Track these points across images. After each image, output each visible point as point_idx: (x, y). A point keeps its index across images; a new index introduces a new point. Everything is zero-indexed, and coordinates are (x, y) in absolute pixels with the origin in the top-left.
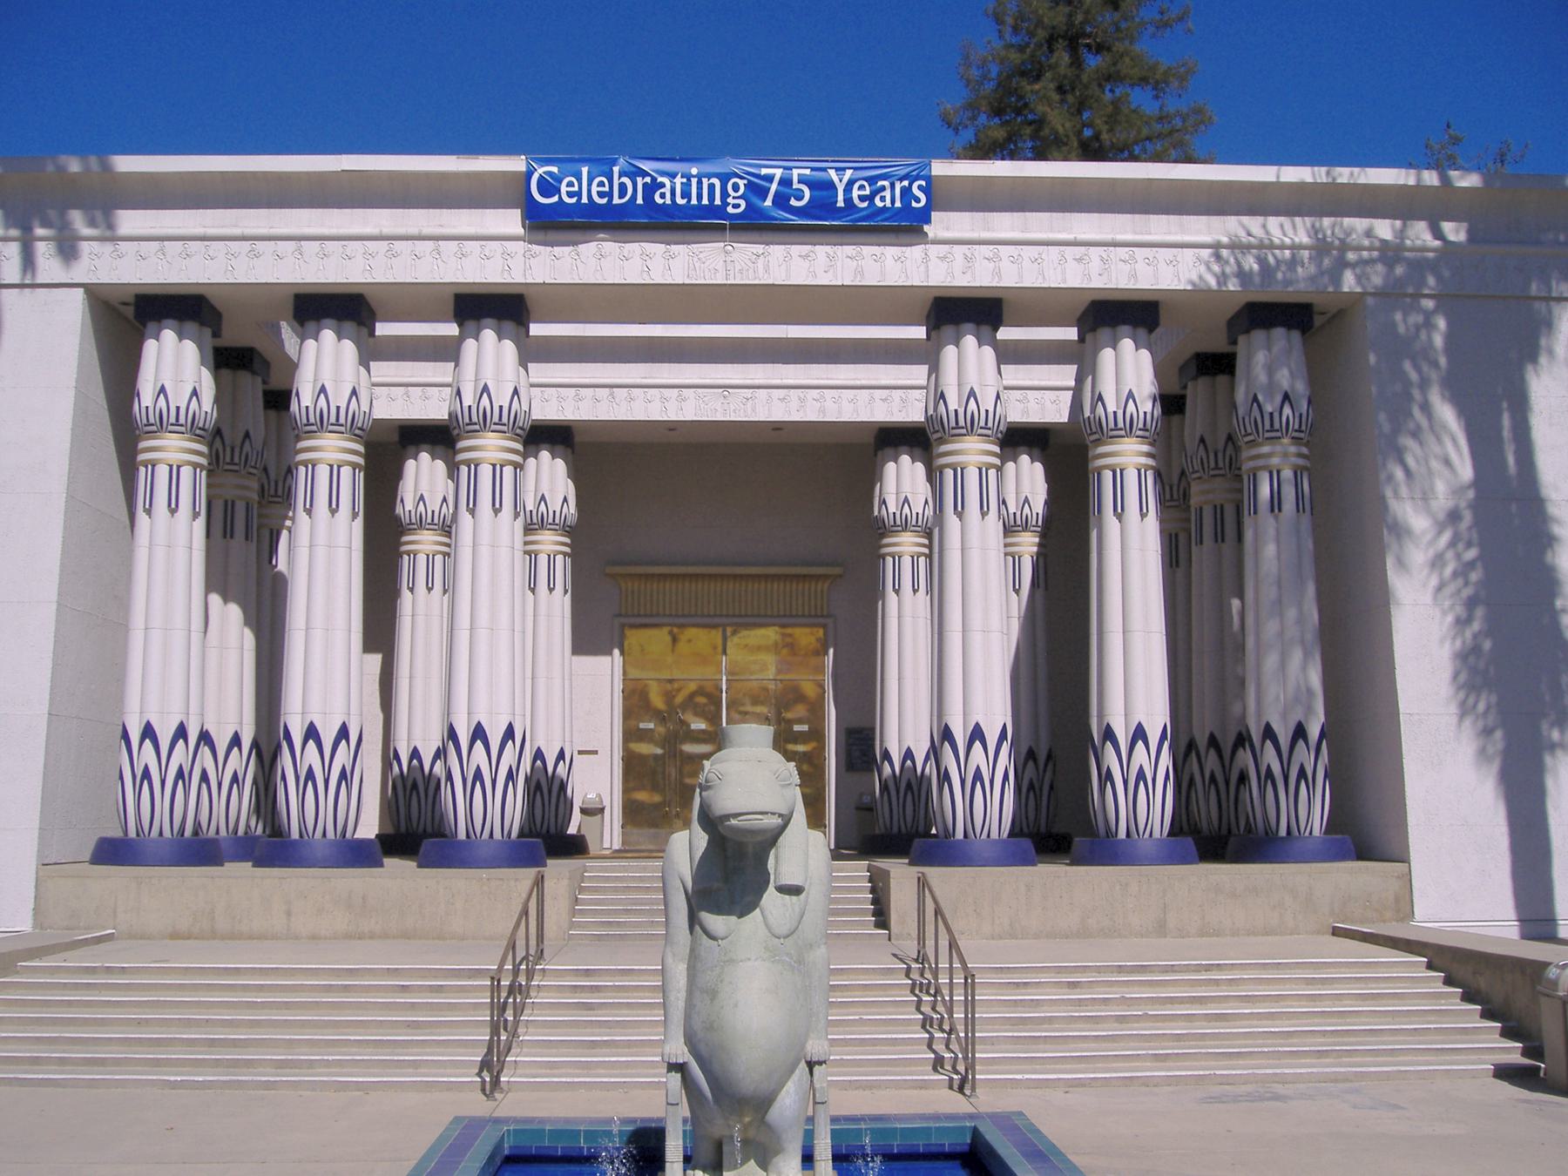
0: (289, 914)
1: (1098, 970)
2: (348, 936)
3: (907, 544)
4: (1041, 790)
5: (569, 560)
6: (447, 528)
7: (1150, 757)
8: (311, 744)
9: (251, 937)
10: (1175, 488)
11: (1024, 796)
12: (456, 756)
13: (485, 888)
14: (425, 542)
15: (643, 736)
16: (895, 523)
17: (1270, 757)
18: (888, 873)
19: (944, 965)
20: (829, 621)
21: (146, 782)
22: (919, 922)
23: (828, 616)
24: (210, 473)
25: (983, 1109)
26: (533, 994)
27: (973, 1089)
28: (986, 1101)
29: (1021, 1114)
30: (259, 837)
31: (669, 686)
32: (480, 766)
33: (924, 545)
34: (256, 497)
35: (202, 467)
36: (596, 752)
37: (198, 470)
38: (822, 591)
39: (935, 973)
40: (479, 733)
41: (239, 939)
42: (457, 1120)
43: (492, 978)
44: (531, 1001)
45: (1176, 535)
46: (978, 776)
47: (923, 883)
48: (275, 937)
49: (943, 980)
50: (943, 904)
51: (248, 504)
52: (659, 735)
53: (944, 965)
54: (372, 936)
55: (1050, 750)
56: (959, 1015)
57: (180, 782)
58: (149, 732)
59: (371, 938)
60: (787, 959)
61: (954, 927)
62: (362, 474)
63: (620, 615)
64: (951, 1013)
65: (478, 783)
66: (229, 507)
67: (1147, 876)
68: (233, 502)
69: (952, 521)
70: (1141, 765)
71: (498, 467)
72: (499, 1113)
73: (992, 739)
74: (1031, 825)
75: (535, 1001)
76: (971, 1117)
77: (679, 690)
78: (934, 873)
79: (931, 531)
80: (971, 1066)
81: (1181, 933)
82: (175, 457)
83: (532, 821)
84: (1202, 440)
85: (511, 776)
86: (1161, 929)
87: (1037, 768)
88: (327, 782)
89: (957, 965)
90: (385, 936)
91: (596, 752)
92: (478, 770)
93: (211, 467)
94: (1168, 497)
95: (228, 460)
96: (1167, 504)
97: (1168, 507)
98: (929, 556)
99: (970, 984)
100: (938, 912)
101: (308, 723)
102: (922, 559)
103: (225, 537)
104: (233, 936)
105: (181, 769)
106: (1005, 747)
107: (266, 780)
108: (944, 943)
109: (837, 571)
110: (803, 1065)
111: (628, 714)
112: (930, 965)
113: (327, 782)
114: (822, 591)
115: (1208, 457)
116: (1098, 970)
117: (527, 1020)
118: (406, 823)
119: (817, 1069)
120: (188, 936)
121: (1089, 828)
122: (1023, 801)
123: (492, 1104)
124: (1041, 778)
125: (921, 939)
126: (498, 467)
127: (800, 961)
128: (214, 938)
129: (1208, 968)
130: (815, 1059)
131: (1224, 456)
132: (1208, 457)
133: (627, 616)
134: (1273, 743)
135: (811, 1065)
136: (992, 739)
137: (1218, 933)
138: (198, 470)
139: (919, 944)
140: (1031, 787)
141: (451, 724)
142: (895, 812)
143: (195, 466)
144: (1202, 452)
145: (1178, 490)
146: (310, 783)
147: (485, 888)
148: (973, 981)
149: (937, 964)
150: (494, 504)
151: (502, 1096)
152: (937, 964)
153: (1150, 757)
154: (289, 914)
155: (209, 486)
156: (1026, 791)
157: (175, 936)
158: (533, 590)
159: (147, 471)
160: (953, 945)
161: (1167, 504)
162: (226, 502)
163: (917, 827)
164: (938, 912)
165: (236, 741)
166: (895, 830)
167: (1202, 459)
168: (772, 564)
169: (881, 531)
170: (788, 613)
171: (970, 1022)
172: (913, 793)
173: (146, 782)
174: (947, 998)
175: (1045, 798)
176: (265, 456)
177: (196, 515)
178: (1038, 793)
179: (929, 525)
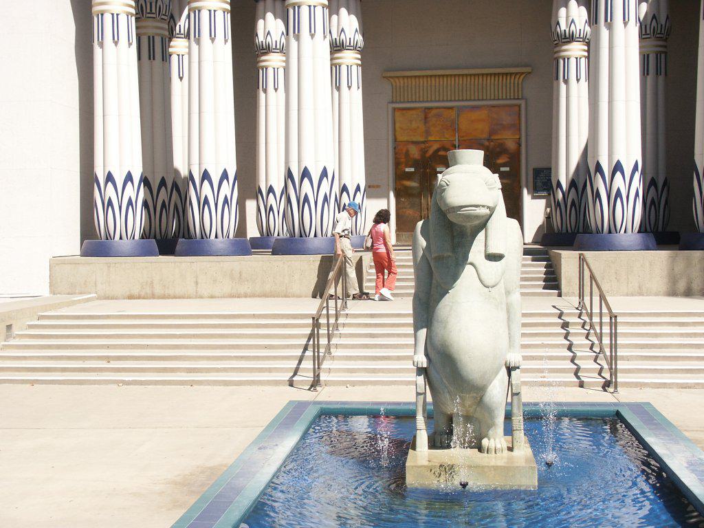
0: (197, 283)
2: (232, 296)
3: (575, 50)
4: (659, 204)
5: (360, 68)
6: (284, 50)
7: (276, 199)
8: (206, 182)
9: (175, 297)
10: (648, 27)
11: (647, 209)
13: (312, 266)
14: (273, 61)
15: (409, 176)
16: (180, 32)
18: (561, 254)
19: (596, 310)
20: (523, 103)
22: (580, 285)
23: (522, 99)
24: (137, 20)
25: (623, 400)
27: (616, 387)
28: (624, 396)
29: (649, 404)
31: (423, 146)
33: (585, 51)
34: (167, 33)
35: (132, 15)
36: (378, 186)
37: (130, 16)
38: (518, 83)
39: (591, 316)
40: (305, 174)
41: (169, 298)
42: (291, 402)
43: (313, 318)
45: (648, 55)
46: (619, 194)
47: (582, 260)
48: (189, 297)
49: (596, 319)
50: (594, 271)
51: (162, 38)
53: (596, 310)
54: (246, 296)
55: (666, 178)
56: (606, 341)
57: (130, 207)
58: (110, 178)
59: (246, 297)
61: (603, 288)
62: (229, 14)
63: (392, 102)
64: (600, 340)
66: (151, 40)
68: (153, 37)
69: (604, 33)
70: (226, 195)
71: (312, 8)
72: (319, 399)
73: (628, 171)
74: (652, 226)
76: (615, 404)
77: (430, 147)
78: (589, 255)
79: (591, 45)
80: (614, 372)
85: (326, 199)
87: (657, 191)
88: (216, 205)
89: (605, 310)
90: (253, 296)
91: (378, 186)
93: (138, 16)
94: (644, 33)
95: (148, 11)
96: (643, 37)
97: (644, 38)
98: (588, 57)
99: (614, 323)
100: (592, 277)
102: (583, 59)
103: (150, 59)
104: (164, 297)
105: (130, 200)
106: (637, 176)
108: (596, 299)
109: (528, 69)
110: (504, 370)
111: (397, 164)
112: (586, 309)
113: (216, 205)
114: (518, 83)
119: (513, 373)
120: (139, 297)
121: (587, 229)
123: (315, 393)
125: (581, 295)
126: (312, 8)
128: (154, 298)
130: (512, 365)
131: (650, 27)
133: (396, 102)
135: (510, 370)
136: (628, 171)
138: (130, 16)
139: (580, 298)
140: (653, 202)
141: (289, 169)
142: (564, 221)
145: (650, 27)
146: (306, 204)
147: (312, 266)
148: (616, 320)
149: (591, 309)
150: (310, 31)
151: (321, 388)
152: (591, 309)
153: (276, 199)
154: (197, 283)
155: (137, 28)
156: (650, 205)
157: (131, 297)
158: (338, 89)
160: (602, 297)
161: (643, 37)
162: (149, 37)
163: (578, 229)
164: (592, 277)
165: (225, 176)
166: (564, 231)
168: (457, 68)
169: (556, 42)
170: (453, 99)
171: (614, 346)
172: (273, 213)
174: (598, 331)
175: (662, 210)
176: (171, 7)
178: (577, 207)
179: (588, 37)
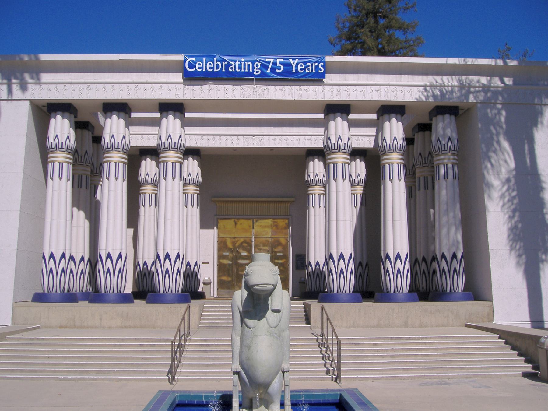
0: (101, 319)
1: (384, 339)
2: (122, 327)
3: (317, 190)
4: (364, 276)
5: (199, 196)
6: (156, 185)
7: (402, 265)
8: (109, 260)
9: (88, 328)
10: (411, 171)
11: (358, 278)
12: (159, 264)
13: (170, 310)
14: (148, 189)
15: (225, 257)
17: (444, 264)
18: (310, 305)
19: (330, 337)
20: (290, 217)
21: (51, 273)
22: (321, 322)
23: (290, 215)
24: (73, 165)
25: (343, 388)
26: (186, 347)
27: (340, 381)
28: (345, 385)
29: (357, 389)
30: (90, 292)
31: (234, 240)
32: (168, 268)
33: (323, 191)
34: (89, 174)
35: (70, 163)
36: (208, 263)
37: (69, 164)
38: (287, 207)
39: (327, 340)
40: (167, 256)
41: (84, 328)
42: (160, 391)
43: (172, 342)
44: (186, 350)
45: (411, 187)
46: (342, 271)
47: (322, 309)
48: (96, 328)
49: (330, 343)
50: (329, 316)
51: (87, 176)
52: (230, 257)
53: (330, 337)
54: (130, 327)
55: (367, 262)
56: (335, 355)
57: (63, 273)
58: (52, 256)
59: (130, 328)
60: (275, 335)
61: (333, 324)
62: (126, 166)
63: (217, 215)
64: (332, 354)
65: (167, 274)
66: (80, 177)
67: (401, 306)
68: (81, 175)
69: (333, 182)
70: (399, 267)
71: (174, 163)
72: (174, 389)
73: (347, 258)
74: (360, 288)
75: (187, 350)
76: (339, 390)
77: (237, 241)
78: (326, 305)
79: (325, 186)
80: (339, 373)
81: (413, 326)
82: (61, 160)
83: (186, 287)
84: (420, 154)
85: (178, 271)
86: (406, 325)
87: (362, 269)
88: (114, 273)
89: (334, 337)
90: (135, 327)
91: (208, 263)
92: (167, 269)
93: (74, 163)
94: (408, 174)
95: (80, 161)
96: (408, 176)
97: (408, 177)
98: (325, 194)
99: (339, 344)
100: (328, 319)
101: (108, 253)
102: (322, 195)
103: (79, 188)
104: (81, 327)
105: (63, 269)
106: (351, 261)
107: (93, 273)
108: (330, 329)
109: (292, 199)
110: (281, 372)
111: (219, 250)
112: (325, 337)
113: (114, 273)
114: (287, 207)
115: (422, 160)
116: (384, 339)
117: (184, 357)
118: (142, 288)
119: (285, 373)
120: (66, 327)
121: (380, 290)
122: (358, 280)
123: (172, 386)
124: (364, 272)
125: (322, 328)
126: (174, 163)
127: (280, 336)
128: (75, 328)
129: (422, 338)
130: (285, 370)
131: (428, 159)
132: (422, 160)
133: (219, 215)
134: (445, 260)
135: (283, 372)
136: (347, 258)
137: (426, 326)
138: (69, 164)
139: (321, 330)
140: (360, 275)
141: (158, 253)
142: (313, 284)
143: (68, 163)
144: (420, 158)
145: (412, 171)
146: (108, 274)
147: (170, 310)
148: (340, 343)
149: (327, 337)
150: (173, 176)
151: (176, 383)
152: (327, 337)
153: (402, 265)
154: (101, 319)
155: (73, 170)
156: (359, 276)
157: (61, 327)
158: (186, 206)
159: (51, 165)
160: (333, 330)
161: (408, 176)
162: (79, 175)
163: (321, 289)
164: (328, 319)
165: (82, 259)
166: (313, 290)
167: (420, 160)
168: (270, 197)
169: (308, 186)
170: (275, 214)
171: (339, 357)
172: (319, 277)
173: (51, 273)
174: (331, 349)
175: (365, 279)
176: (93, 159)
177: (68, 180)
178: (363, 277)
179: (325, 184)
